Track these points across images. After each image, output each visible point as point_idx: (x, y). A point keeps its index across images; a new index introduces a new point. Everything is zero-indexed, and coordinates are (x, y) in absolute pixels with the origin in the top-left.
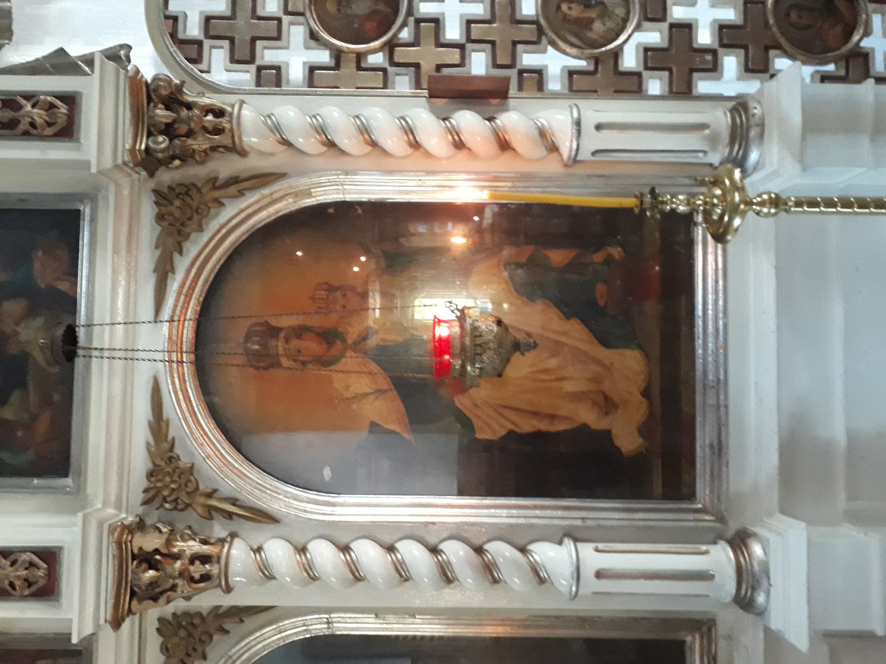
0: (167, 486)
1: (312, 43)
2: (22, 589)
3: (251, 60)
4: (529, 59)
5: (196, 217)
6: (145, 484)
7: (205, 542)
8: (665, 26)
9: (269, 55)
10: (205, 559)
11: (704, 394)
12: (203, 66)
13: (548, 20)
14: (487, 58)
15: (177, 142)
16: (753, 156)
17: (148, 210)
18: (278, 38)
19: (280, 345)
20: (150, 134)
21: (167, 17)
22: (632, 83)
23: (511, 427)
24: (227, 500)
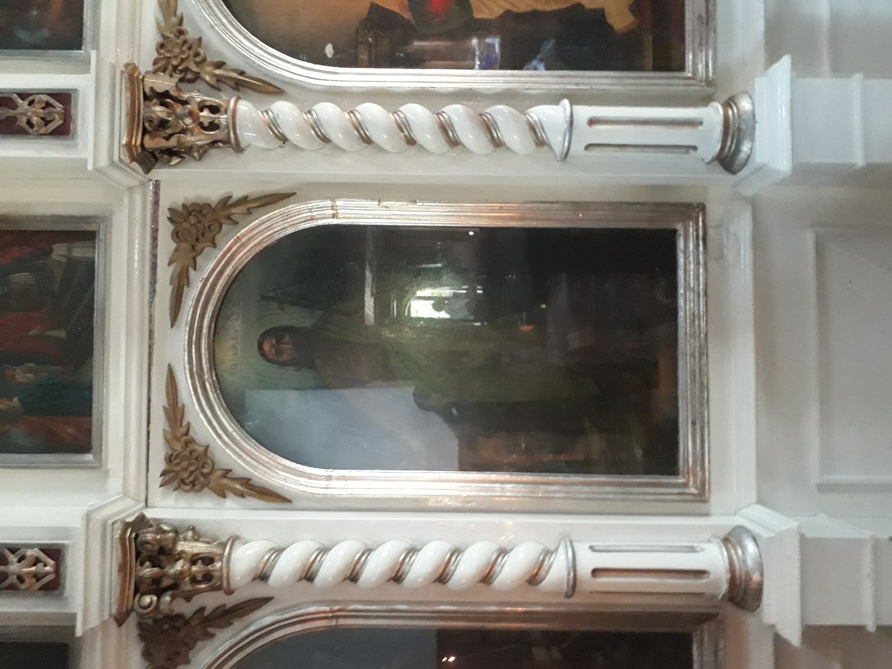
0: (176, 57)
6: (155, 55)
24: (234, 71)
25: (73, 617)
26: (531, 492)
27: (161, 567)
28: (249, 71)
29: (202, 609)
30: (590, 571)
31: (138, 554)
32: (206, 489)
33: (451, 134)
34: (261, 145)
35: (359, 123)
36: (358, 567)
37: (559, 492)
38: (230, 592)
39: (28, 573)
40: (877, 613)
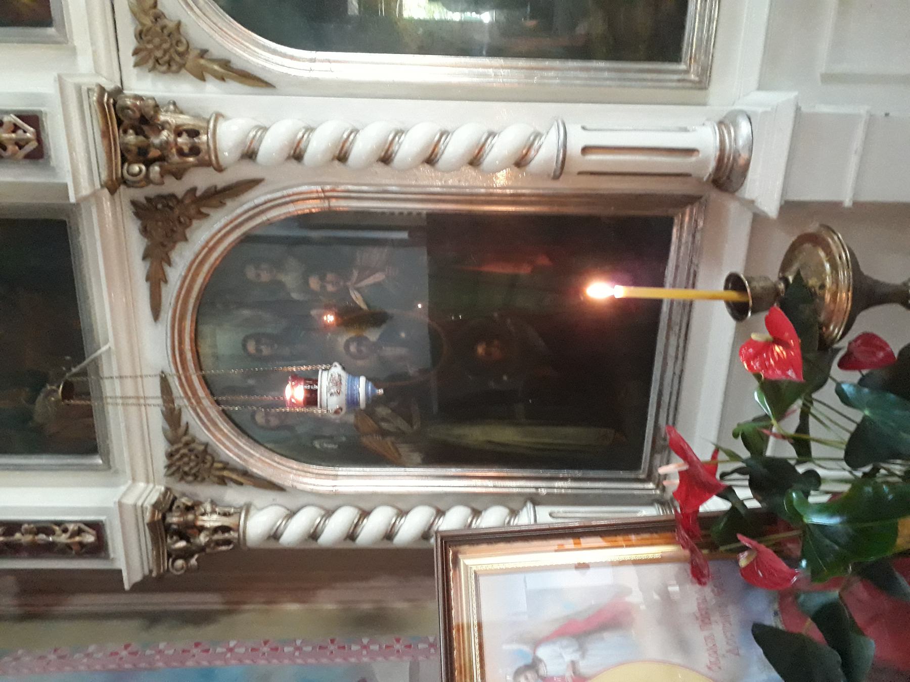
5: (179, 229)
7: (225, 514)
10: (225, 529)
11: (681, 321)
17: (132, 229)
26: (526, 78)
27: (147, 137)
29: (194, 190)
30: (580, 151)
31: (120, 123)
32: (183, 71)
36: (348, 144)
37: (555, 78)
38: (220, 169)
39: (11, 139)
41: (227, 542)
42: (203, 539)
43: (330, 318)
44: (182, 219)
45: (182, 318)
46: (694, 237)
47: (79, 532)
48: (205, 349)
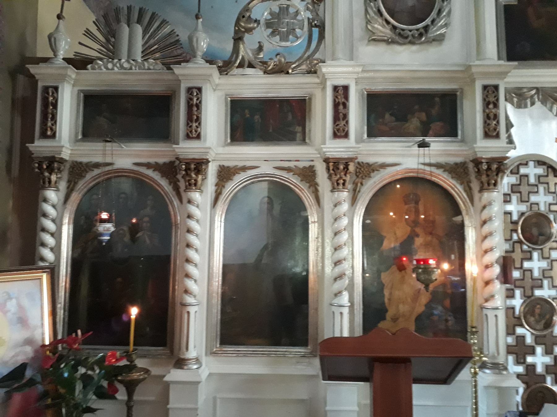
0: (364, 169)
1: (520, 214)
2: (336, 128)
3: (513, 192)
4: (518, 293)
8: (533, 344)
9: (514, 198)
10: (50, 182)
12: (510, 175)
13: (533, 300)
14: (518, 277)
15: (485, 172)
16: (487, 371)
17: (459, 160)
18: (522, 201)
19: (413, 205)
20: (487, 162)
21: (527, 162)
22: (511, 332)
23: (386, 285)
24: (360, 189)
25: (178, 144)
28: (360, 194)
29: (179, 181)
33: (338, 263)
34: (333, 199)
35: (341, 232)
38: (185, 191)
40: (172, 408)
41: (44, 183)
42: (47, 174)
43: (134, 221)
44: (169, 176)
45: (135, 174)
46: (159, 355)
47: (52, 129)
48: (123, 179)
